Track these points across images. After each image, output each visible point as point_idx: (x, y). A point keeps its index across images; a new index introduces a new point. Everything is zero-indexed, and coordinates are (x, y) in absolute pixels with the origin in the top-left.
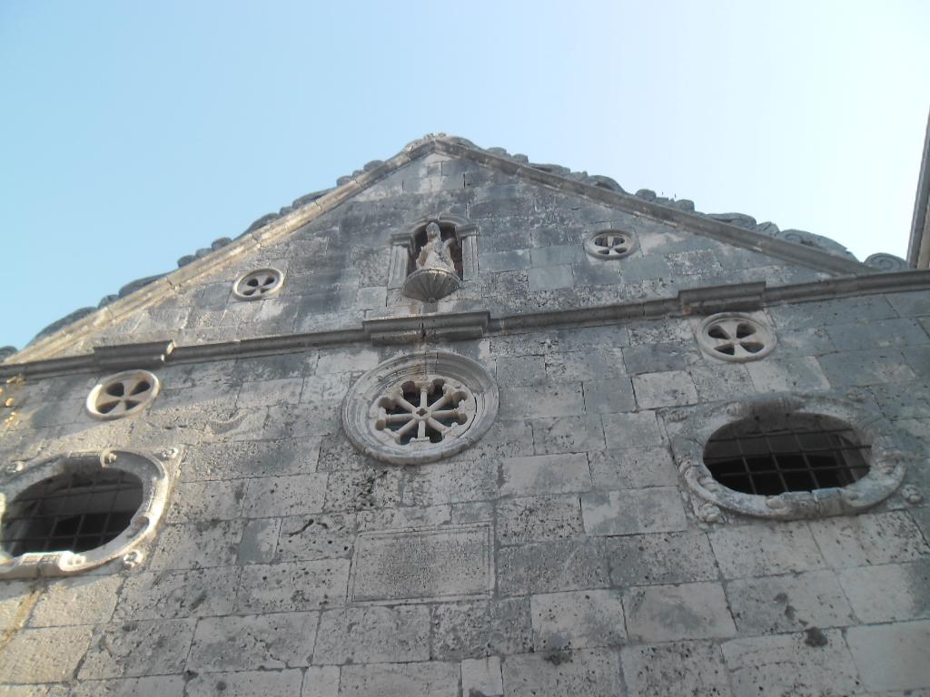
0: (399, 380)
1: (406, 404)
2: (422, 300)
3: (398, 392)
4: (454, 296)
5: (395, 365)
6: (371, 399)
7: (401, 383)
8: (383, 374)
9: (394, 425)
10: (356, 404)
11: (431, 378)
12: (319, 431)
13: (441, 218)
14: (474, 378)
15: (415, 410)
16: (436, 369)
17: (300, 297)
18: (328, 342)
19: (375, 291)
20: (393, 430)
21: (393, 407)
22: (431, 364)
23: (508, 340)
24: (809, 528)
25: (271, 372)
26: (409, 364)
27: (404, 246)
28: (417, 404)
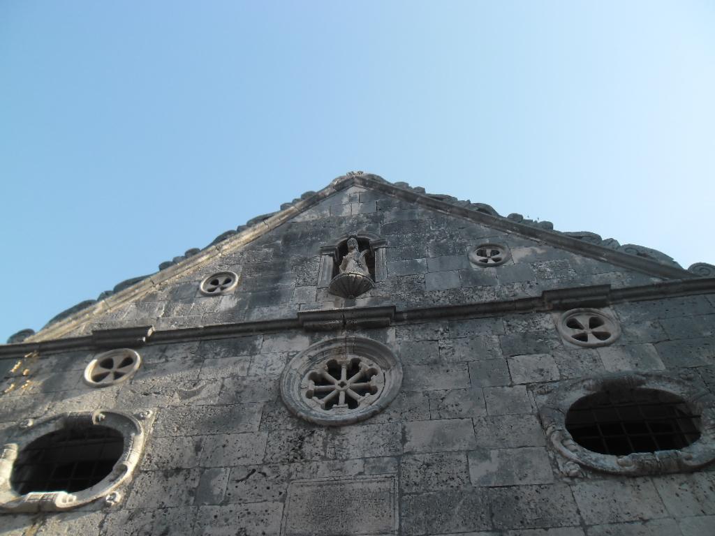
5: (322, 347)
6: (302, 373)
8: (312, 354)
13: (358, 235)
15: (337, 382)
16: (354, 351)
23: (410, 328)
27: (330, 255)
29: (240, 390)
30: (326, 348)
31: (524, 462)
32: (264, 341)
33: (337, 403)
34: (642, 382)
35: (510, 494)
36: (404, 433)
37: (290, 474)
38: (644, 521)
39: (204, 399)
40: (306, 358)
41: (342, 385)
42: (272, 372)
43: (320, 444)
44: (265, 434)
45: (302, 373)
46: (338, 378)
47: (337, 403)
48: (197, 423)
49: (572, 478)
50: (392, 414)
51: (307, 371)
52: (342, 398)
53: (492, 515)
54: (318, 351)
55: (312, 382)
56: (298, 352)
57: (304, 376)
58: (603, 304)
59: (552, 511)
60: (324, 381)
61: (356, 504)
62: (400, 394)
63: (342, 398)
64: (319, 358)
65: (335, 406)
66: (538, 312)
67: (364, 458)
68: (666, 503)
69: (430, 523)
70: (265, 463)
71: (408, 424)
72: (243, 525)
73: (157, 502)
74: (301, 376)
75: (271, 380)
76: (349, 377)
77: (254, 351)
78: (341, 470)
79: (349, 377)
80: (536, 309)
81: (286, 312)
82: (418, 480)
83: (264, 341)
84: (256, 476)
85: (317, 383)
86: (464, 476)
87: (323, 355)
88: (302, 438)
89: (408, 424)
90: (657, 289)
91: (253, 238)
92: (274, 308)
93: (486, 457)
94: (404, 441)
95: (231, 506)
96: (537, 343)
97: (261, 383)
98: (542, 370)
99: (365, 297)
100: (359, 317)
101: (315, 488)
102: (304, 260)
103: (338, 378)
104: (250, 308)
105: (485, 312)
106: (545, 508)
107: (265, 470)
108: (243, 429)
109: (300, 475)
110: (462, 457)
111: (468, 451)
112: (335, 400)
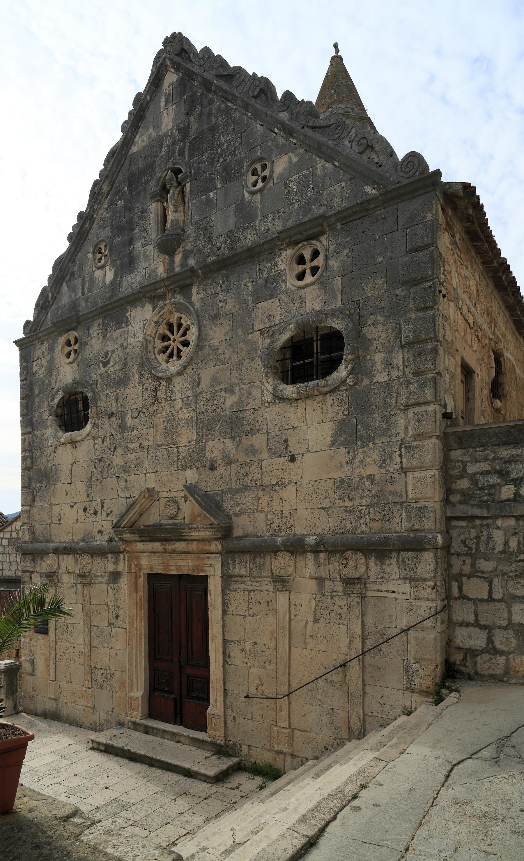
8: (155, 319)
16: (178, 310)
27: (158, 201)
30: (162, 312)
31: (250, 394)
34: (321, 321)
35: (241, 415)
36: (199, 378)
37: (154, 412)
38: (294, 428)
39: (112, 366)
40: (153, 324)
43: (164, 391)
44: (141, 388)
46: (169, 339)
48: (113, 384)
49: (269, 403)
50: (194, 365)
51: (155, 334)
53: (232, 429)
54: (158, 317)
55: (162, 355)
58: (316, 237)
59: (256, 425)
60: (167, 348)
61: (180, 427)
66: (279, 249)
67: (182, 398)
68: (308, 417)
69: (207, 435)
70: (144, 406)
71: (200, 372)
72: (140, 442)
76: (172, 333)
78: (173, 407)
79: (172, 333)
80: (278, 248)
82: (204, 410)
84: (141, 414)
85: (164, 353)
86: (223, 405)
88: (156, 388)
89: (200, 372)
93: (233, 392)
94: (199, 384)
95: (135, 433)
96: (269, 288)
98: (270, 315)
101: (164, 419)
103: (169, 339)
105: (94, 316)
106: (254, 423)
107: (144, 410)
108: (132, 385)
109: (158, 412)
110: (223, 393)
111: (226, 389)
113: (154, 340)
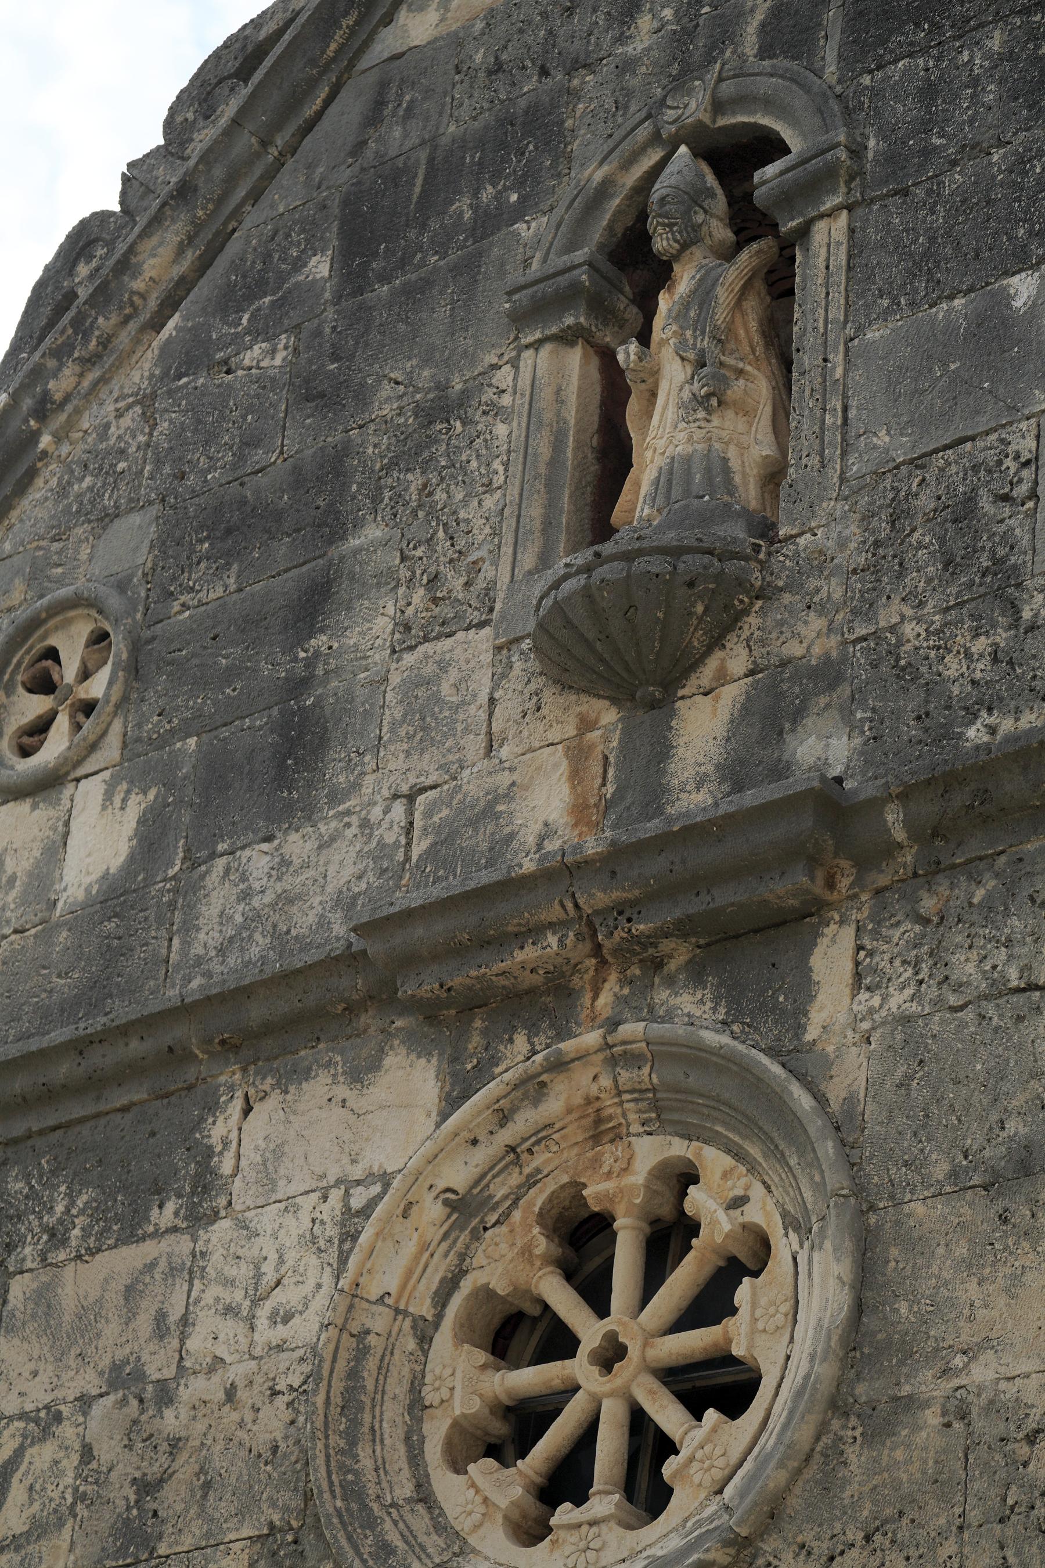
0: (531, 1182)
1: (529, 1379)
2: (614, 701)
3: (526, 1252)
4: (736, 658)
5: (504, 1118)
6: (424, 1308)
7: (538, 1198)
8: (458, 1175)
9: (567, 1481)
10: (362, 1352)
11: (650, 1152)
12: (240, 1514)
13: (718, 107)
14: (783, 1160)
15: (579, 1368)
16: (663, 1112)
17: (192, 741)
18: (297, 1016)
19: (443, 666)
20: (580, 1499)
21: (499, 1428)
22: (639, 1092)
23: (928, 904)
24: (526, 1476)
25: (96, 1211)
26: (553, 1106)
27: (566, 338)
28: (560, 1343)
29: (154, 1471)
32: (247, 1110)
33: (667, 1447)
41: (612, 1354)
42: (281, 1332)
45: (424, 1308)
47: (667, 1447)
52: (668, 1415)
54: (481, 1156)
56: (386, 1180)
57: (437, 1325)
62: (836, 1424)
63: (668, 1415)
64: (500, 1190)
65: (669, 1468)
73: (429, 1115)
74: (418, 1321)
75: (275, 1393)
77: (203, 1196)
81: (349, 871)
83: (247, 1110)
87: (517, 1162)
90: (423, 1556)
91: (190, 256)
92: (297, 845)
97: (235, 1416)
99: (723, 678)
100: (654, 897)
102: (442, 409)
104: (192, 862)
112: (649, 1446)
113: (425, 1340)
